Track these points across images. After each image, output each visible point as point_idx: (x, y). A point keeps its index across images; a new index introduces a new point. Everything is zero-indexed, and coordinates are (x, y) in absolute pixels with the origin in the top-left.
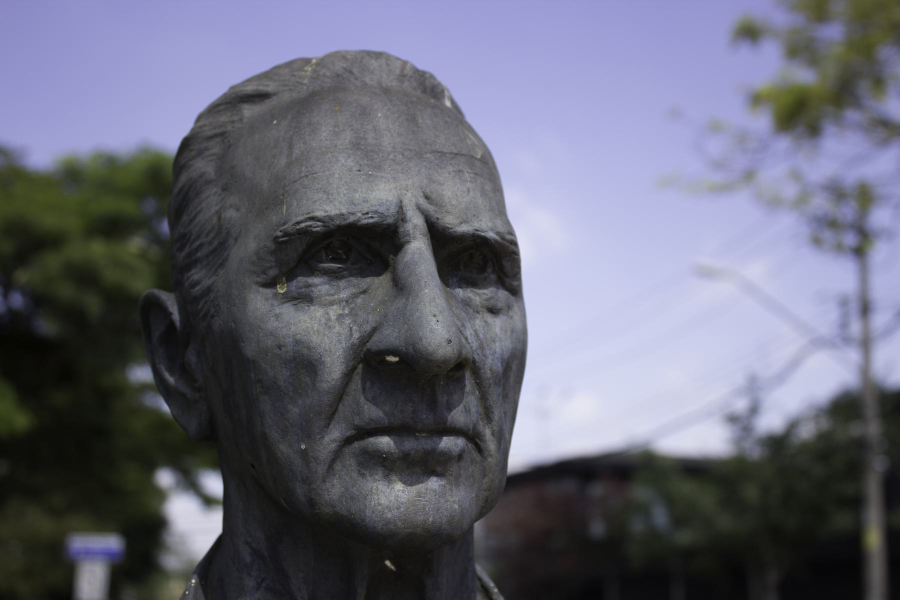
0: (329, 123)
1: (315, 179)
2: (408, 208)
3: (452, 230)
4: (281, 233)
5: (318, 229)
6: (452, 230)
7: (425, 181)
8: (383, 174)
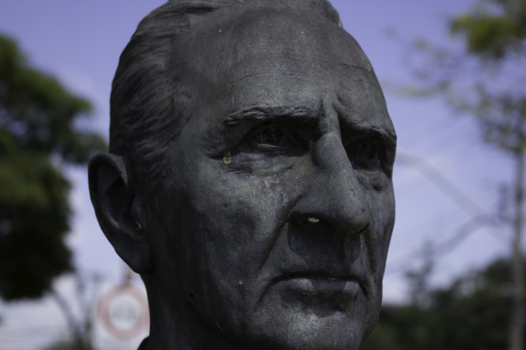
3: (357, 125)
4: (231, 118)
5: (261, 117)
6: (357, 125)
7: (338, 86)
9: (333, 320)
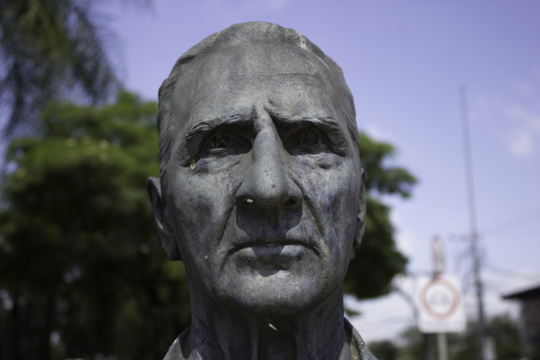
0: (217, 67)
1: (206, 100)
2: (258, 110)
3: (288, 120)
5: (206, 129)
6: (288, 120)
7: (270, 92)
8: (244, 92)
9: (276, 278)
